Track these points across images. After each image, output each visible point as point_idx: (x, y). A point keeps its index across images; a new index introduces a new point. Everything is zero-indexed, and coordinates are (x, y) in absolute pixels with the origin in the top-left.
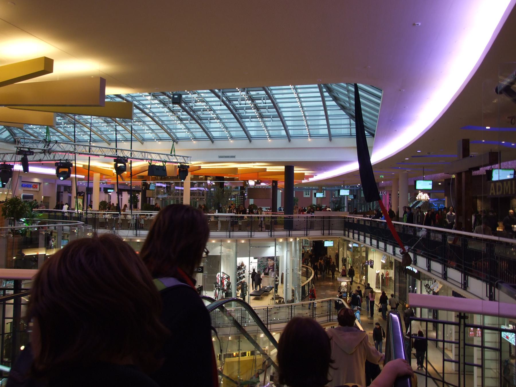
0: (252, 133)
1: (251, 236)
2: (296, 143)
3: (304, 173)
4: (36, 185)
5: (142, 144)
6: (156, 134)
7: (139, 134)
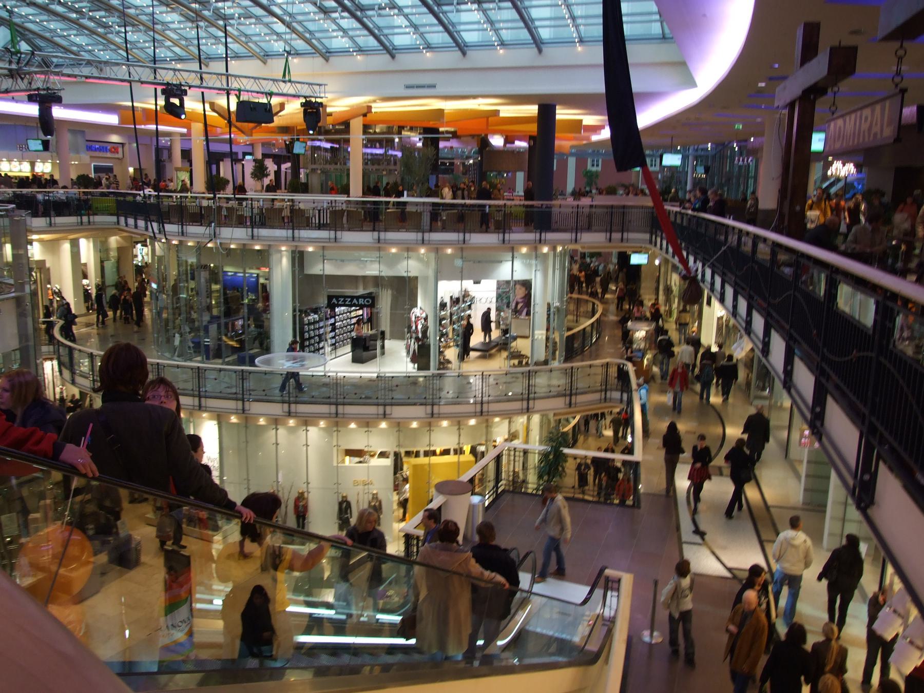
0: (545, 34)
1: (293, 237)
2: (553, 55)
3: (581, 121)
4: (115, 147)
5: (265, 63)
6: (351, 38)
7: (256, 43)
